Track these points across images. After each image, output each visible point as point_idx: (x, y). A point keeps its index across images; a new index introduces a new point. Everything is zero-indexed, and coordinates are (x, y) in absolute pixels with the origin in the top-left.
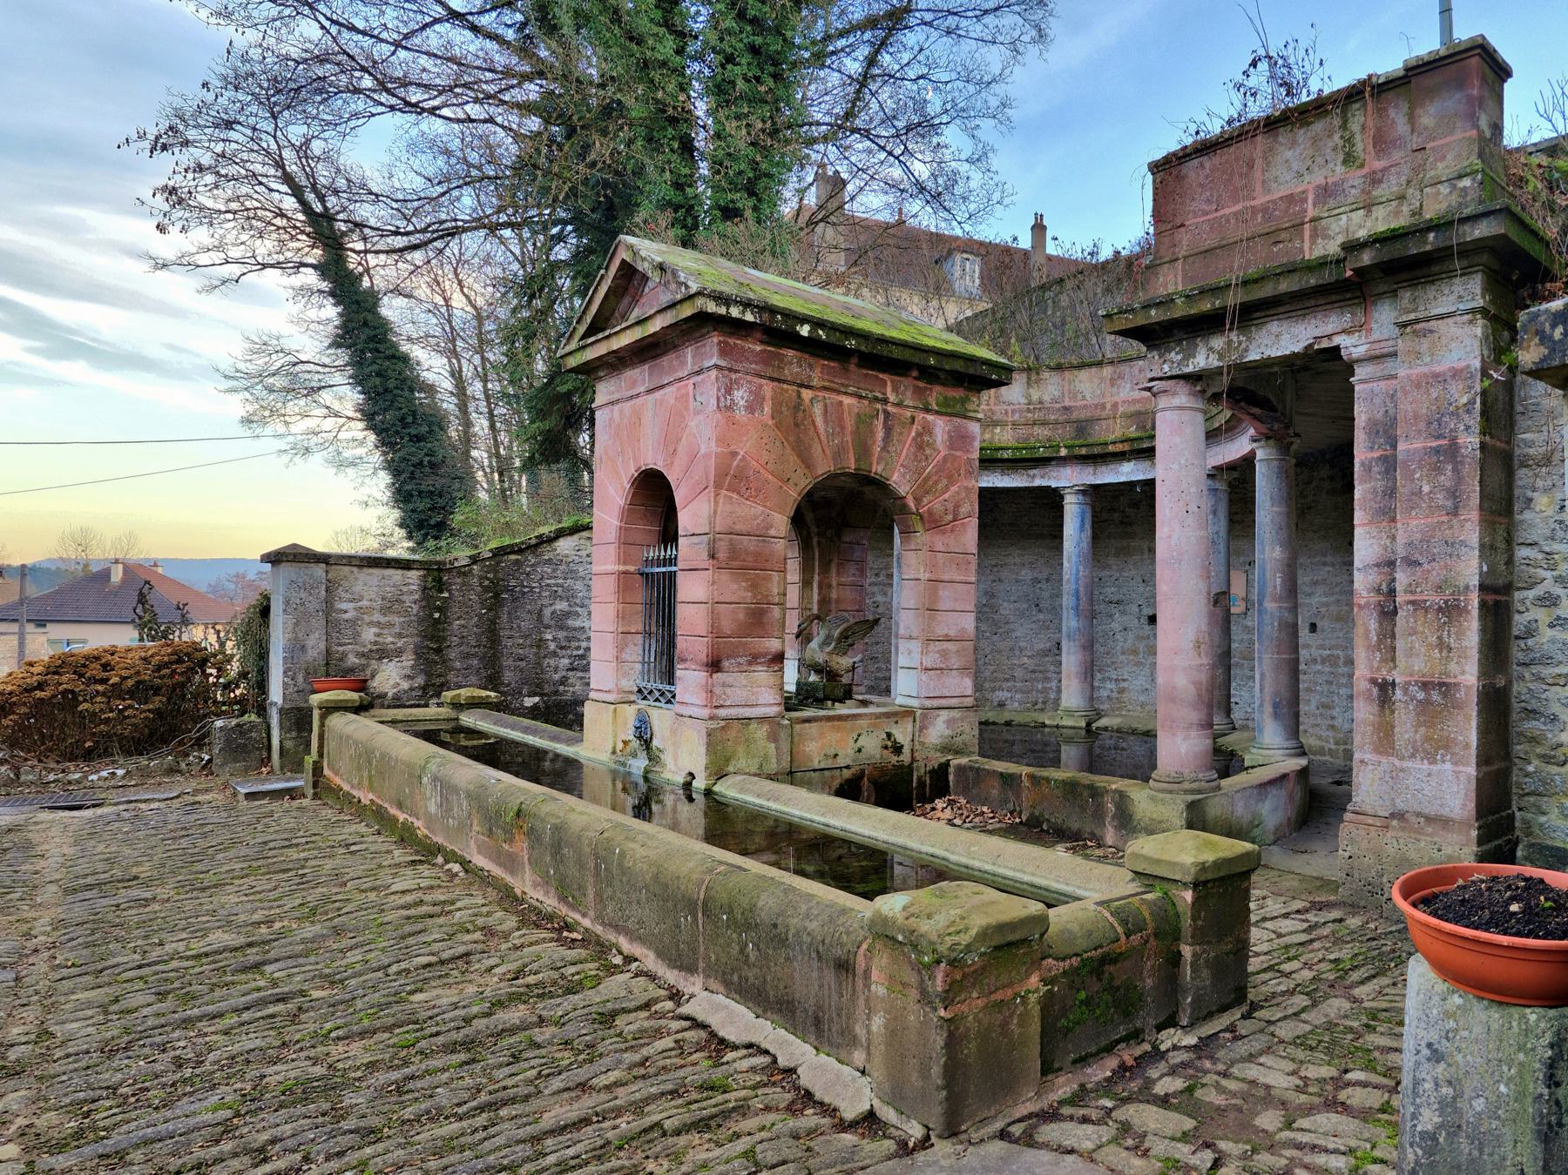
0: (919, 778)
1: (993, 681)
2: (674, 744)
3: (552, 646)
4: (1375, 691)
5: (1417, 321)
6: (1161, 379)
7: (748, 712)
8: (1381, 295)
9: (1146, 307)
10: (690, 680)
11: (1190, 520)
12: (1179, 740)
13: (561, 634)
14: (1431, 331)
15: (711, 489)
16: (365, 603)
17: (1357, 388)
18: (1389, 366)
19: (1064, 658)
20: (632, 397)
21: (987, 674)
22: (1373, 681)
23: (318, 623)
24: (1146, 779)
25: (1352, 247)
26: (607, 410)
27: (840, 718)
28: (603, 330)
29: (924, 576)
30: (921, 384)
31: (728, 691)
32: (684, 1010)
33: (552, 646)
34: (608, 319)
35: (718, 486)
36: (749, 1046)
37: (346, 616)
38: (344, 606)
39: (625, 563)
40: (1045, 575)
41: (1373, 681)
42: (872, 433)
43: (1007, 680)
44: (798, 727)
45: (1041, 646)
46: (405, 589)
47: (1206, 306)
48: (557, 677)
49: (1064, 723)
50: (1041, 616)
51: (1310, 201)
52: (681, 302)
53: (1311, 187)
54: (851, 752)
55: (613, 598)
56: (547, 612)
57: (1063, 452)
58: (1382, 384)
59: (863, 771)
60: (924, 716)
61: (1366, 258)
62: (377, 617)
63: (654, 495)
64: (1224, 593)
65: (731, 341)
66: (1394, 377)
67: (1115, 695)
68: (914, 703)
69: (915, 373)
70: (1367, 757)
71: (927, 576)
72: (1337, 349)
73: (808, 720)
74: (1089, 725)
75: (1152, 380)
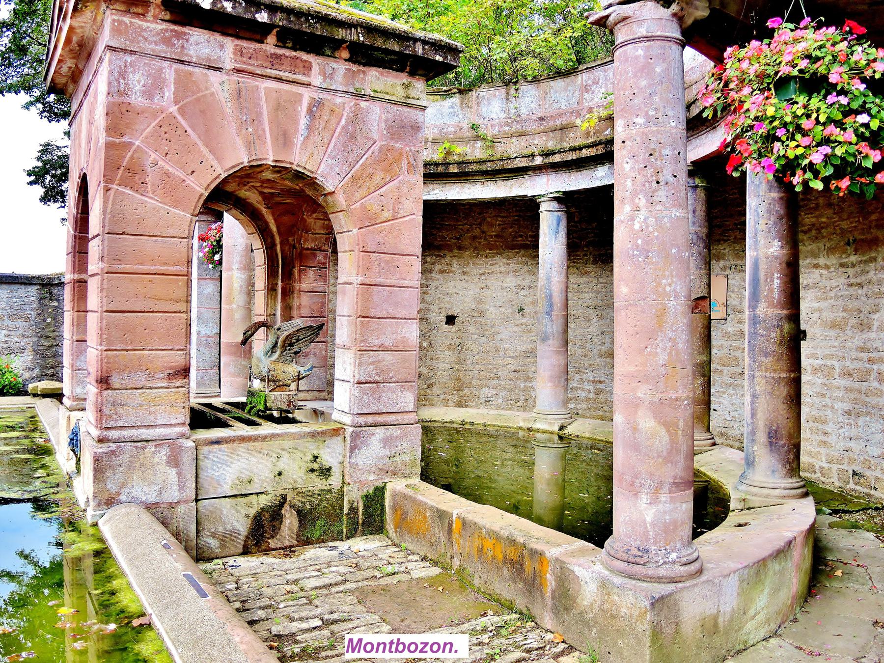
0: (351, 503)
1: (479, 379)
7: (144, 433)
12: (644, 499)
29: (357, 279)
30: (355, 67)
31: (120, 410)
40: (526, 283)
42: (295, 121)
44: (205, 449)
45: (524, 348)
46: (26, 300)
50: (524, 320)
54: (269, 475)
57: (538, 161)
60: (356, 436)
64: (703, 298)
65: (127, 19)
67: (592, 395)
68: (347, 419)
69: (345, 54)
71: (360, 279)
73: (217, 442)
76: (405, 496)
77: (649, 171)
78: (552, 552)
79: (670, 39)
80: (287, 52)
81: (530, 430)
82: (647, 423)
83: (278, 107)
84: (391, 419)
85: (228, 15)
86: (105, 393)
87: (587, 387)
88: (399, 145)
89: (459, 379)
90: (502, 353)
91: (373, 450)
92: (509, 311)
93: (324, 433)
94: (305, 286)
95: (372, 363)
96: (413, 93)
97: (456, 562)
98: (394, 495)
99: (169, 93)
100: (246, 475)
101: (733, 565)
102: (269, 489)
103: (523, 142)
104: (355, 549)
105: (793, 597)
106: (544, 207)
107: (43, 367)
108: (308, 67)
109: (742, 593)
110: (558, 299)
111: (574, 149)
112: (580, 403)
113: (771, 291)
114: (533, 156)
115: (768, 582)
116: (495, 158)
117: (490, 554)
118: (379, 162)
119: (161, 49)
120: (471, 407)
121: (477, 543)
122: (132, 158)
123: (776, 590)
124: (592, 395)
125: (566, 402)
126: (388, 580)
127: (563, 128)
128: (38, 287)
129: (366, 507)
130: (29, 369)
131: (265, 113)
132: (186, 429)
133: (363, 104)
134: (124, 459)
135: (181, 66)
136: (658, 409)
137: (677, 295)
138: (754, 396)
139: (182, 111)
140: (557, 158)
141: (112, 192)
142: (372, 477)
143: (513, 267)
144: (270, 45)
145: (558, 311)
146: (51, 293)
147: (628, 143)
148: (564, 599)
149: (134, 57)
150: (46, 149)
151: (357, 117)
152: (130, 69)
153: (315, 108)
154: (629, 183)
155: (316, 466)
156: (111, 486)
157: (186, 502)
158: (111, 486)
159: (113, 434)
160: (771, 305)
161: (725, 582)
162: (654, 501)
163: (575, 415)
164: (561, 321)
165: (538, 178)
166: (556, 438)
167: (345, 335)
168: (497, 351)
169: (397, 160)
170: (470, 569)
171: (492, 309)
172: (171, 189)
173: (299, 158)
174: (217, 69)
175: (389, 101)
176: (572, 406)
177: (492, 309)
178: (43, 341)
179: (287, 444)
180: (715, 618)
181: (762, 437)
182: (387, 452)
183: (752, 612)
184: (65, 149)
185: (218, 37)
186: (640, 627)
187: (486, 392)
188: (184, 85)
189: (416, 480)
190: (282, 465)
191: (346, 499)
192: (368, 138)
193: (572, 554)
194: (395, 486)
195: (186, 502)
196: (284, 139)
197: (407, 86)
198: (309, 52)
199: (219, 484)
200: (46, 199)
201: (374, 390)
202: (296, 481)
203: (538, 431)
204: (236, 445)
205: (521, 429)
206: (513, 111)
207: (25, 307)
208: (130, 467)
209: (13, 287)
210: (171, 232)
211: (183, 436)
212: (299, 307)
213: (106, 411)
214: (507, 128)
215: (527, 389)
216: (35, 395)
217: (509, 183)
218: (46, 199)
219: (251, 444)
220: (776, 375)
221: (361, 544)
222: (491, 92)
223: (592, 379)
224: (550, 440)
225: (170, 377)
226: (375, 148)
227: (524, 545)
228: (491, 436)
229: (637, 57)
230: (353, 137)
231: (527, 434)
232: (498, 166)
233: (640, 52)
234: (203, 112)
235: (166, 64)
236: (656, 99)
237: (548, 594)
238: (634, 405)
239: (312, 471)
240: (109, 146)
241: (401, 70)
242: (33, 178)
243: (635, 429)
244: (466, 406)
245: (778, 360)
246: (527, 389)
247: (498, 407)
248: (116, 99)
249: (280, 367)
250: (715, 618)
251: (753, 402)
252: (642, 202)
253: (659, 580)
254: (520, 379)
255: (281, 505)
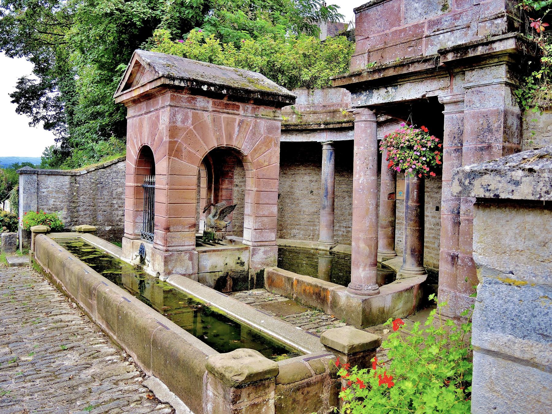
0: (251, 276)
2: (153, 260)
3: (116, 206)
4: (450, 258)
5: (474, 87)
6: (357, 107)
8: (457, 73)
9: (351, 76)
10: (159, 232)
11: (368, 172)
12: (361, 269)
13: (119, 201)
14: (481, 92)
15: (167, 156)
16: (50, 189)
17: (445, 116)
18: (459, 107)
19: (321, 218)
20: (140, 115)
21: (289, 222)
22: (449, 254)
23: (35, 197)
24: (346, 286)
25: (443, 52)
26: (131, 120)
27: (218, 251)
28: (129, 88)
29: (255, 189)
31: (173, 240)
32: (145, 383)
33: (116, 206)
34: (132, 83)
35: (170, 155)
36: (167, 403)
37: (44, 194)
38: (43, 190)
39: (137, 183)
40: (315, 179)
41: (449, 254)
42: (234, 129)
43: (298, 225)
45: (313, 210)
47: (376, 76)
48: (118, 219)
49: (320, 247)
50: (313, 197)
51: (426, 27)
52: (156, 79)
53: (426, 21)
54: (222, 264)
55: (132, 196)
56: (114, 192)
57: (323, 126)
58: (457, 115)
59: (228, 273)
60: (254, 250)
61: (450, 57)
62: (54, 194)
63: (146, 156)
65: (175, 94)
66: (463, 112)
67: (345, 233)
68: (250, 244)
69: (252, 102)
70: (445, 289)
71: (256, 189)
72: (436, 97)
73: (205, 252)
74: (331, 248)
75: (353, 107)
76: (273, 273)
77: (365, 164)
78: (330, 289)
79: (373, 121)
80: (231, 102)
81: (317, 249)
82: (362, 245)
83: (228, 124)
84: (266, 243)
85: (213, 92)
86: (168, 233)
87: (342, 230)
88: (271, 136)
89: (281, 225)
90: (302, 213)
91: (260, 256)
92: (306, 192)
93: (242, 249)
94: (224, 187)
95: (260, 222)
96: (277, 115)
97: (295, 296)
98: (268, 273)
99: (190, 121)
100: (214, 264)
101: (390, 292)
102: (222, 270)
103: (315, 116)
104: (254, 293)
105: (414, 307)
106: (325, 147)
107: (72, 217)
108: (238, 107)
109: (393, 301)
110: (330, 190)
111: (339, 123)
112: (339, 237)
113: (413, 196)
114: (320, 124)
115: (403, 299)
116: (302, 124)
117: (308, 291)
118: (263, 143)
119: (187, 104)
120: (287, 239)
121: (303, 288)
122: (178, 146)
123: (406, 303)
124: (345, 233)
125: (333, 237)
126: (270, 302)
127: (334, 112)
128: (70, 177)
129: (257, 277)
130: (65, 218)
131: (223, 126)
132: (194, 247)
133: (258, 120)
134: (174, 258)
135: (194, 111)
136: (365, 241)
137: (373, 205)
138: (406, 236)
139: (194, 128)
140: (331, 126)
141: (171, 160)
142: (260, 266)
143: (308, 171)
144: (225, 101)
145: (330, 195)
146: (76, 180)
147: (358, 155)
148: (334, 304)
149: (178, 109)
150: (22, 81)
151: (256, 125)
152: (177, 113)
153: (241, 122)
154: (358, 167)
155: (239, 261)
156: (170, 268)
157: (195, 274)
158: (170, 268)
159: (170, 248)
160: (413, 202)
161: (387, 297)
162: (364, 270)
163: (337, 243)
164: (331, 200)
165: (322, 134)
166: (328, 253)
167: (249, 211)
168: (300, 211)
169: (270, 142)
170: (300, 298)
171: (297, 191)
172: (191, 157)
173: (235, 144)
174: (206, 111)
175: (268, 119)
176: (335, 238)
177: (297, 191)
178: (72, 204)
179: (229, 253)
180: (384, 308)
181: (409, 252)
182: (265, 257)
183: (397, 308)
184: (34, 82)
185: (207, 99)
186: (359, 309)
187: (294, 231)
188: (195, 118)
189: (276, 268)
190: (227, 261)
191: (250, 274)
192: (260, 134)
193: (337, 289)
194: (268, 270)
195: (195, 274)
196: (230, 136)
197: (274, 112)
198: (238, 102)
199: (205, 268)
200: (18, 111)
201: (261, 233)
202: (232, 267)
203: (320, 250)
204: (211, 253)
205: (312, 249)
206: (311, 101)
207: (63, 187)
208: (176, 261)
209: (57, 177)
210: (191, 174)
211: (194, 249)
212: (221, 196)
213: (168, 240)
214: (308, 109)
215: (314, 230)
216: (80, 232)
217: (308, 135)
218: (18, 111)
219: (217, 253)
220: (414, 228)
221: (256, 292)
222: (301, 91)
223: (345, 226)
224: (326, 254)
225: (190, 227)
226: (262, 137)
227: (321, 287)
228: (296, 252)
229: (362, 127)
230: (254, 134)
231: (315, 251)
232: (304, 127)
233: (363, 125)
234: (202, 128)
235: (189, 110)
236: (367, 141)
237: (329, 303)
238: (358, 239)
239: (238, 263)
240: (170, 142)
241: (273, 106)
242: (14, 99)
243: (359, 247)
244: (284, 238)
245: (415, 223)
246: (314, 230)
247: (300, 239)
248: (172, 124)
249: (219, 222)
250: (384, 308)
251: (406, 238)
252: (362, 174)
253: (365, 295)
254: (311, 225)
255: (227, 276)
